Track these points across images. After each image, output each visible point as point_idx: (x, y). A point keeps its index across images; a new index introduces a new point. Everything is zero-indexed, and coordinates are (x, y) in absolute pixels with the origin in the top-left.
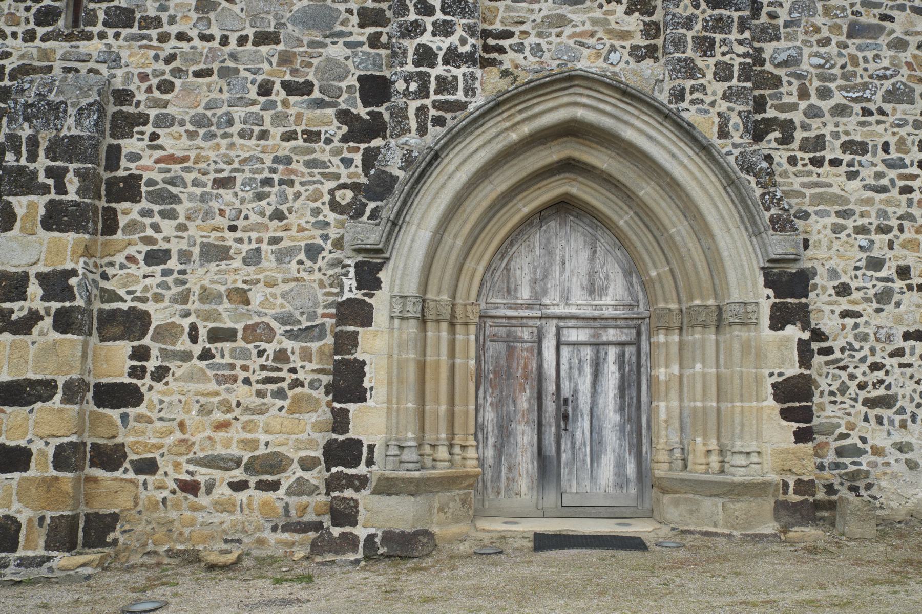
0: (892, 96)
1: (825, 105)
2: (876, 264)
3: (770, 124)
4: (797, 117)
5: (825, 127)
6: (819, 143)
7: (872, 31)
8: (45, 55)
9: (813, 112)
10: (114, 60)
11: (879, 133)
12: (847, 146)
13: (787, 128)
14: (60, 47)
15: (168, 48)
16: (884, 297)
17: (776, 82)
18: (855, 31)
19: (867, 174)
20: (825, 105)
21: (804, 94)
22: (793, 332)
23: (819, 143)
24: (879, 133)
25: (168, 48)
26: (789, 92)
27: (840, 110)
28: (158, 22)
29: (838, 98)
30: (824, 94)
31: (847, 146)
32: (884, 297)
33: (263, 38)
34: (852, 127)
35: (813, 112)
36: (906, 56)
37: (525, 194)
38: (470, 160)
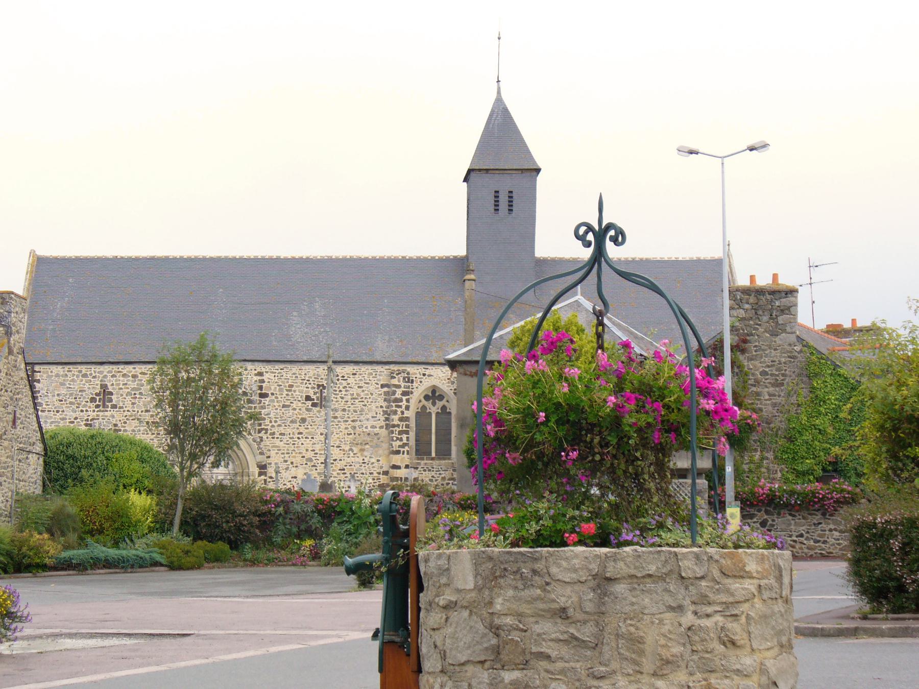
0: (292, 422)
1: (276, 425)
2: (286, 461)
3: (262, 429)
4: (269, 427)
5: (275, 430)
6: (274, 433)
7: (289, 406)
8: (98, 415)
9: (273, 426)
10: (113, 417)
11: (289, 430)
12: (281, 434)
13: (267, 430)
14: (101, 414)
15: (125, 414)
16: (287, 469)
17: (264, 419)
18: (284, 406)
19: (285, 441)
20: (276, 425)
21: (271, 422)
22: (263, 477)
23: (274, 433)
24: (289, 430)
25: (125, 414)
26: (267, 422)
27: (279, 426)
28: (122, 408)
29: (279, 423)
30: (276, 422)
31: (281, 434)
32: (287, 469)
33: (147, 411)
34: (282, 429)
35: (273, 426)
36: (296, 412)
37: (71, 572)
38: (415, 361)
